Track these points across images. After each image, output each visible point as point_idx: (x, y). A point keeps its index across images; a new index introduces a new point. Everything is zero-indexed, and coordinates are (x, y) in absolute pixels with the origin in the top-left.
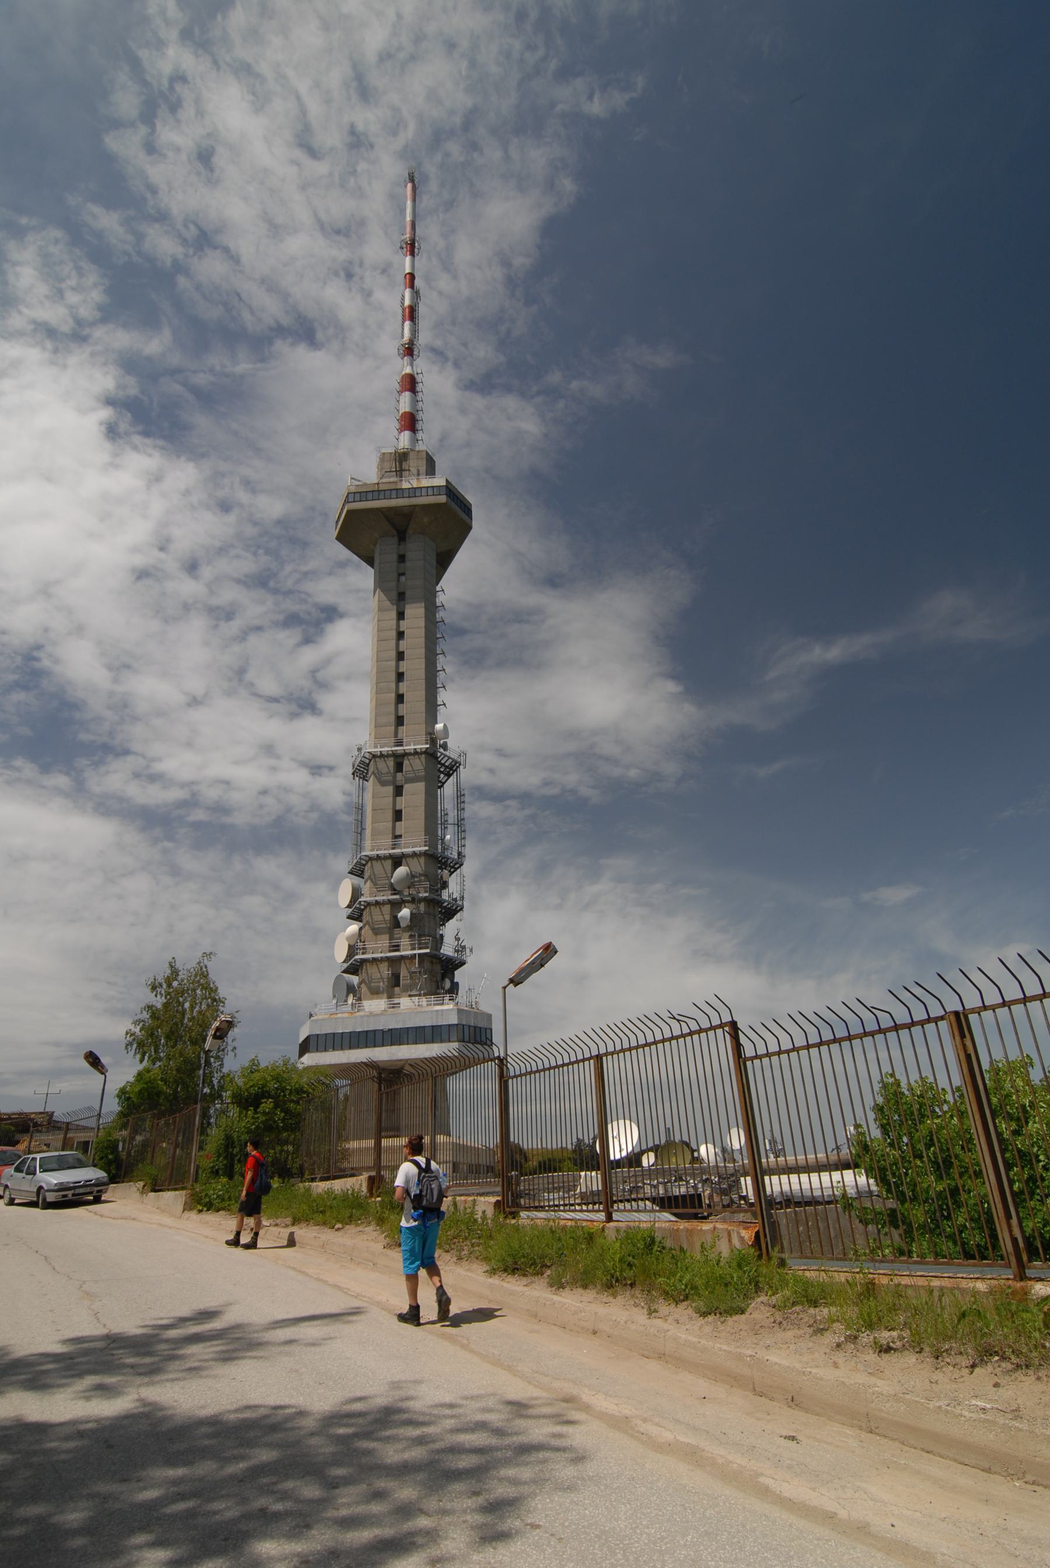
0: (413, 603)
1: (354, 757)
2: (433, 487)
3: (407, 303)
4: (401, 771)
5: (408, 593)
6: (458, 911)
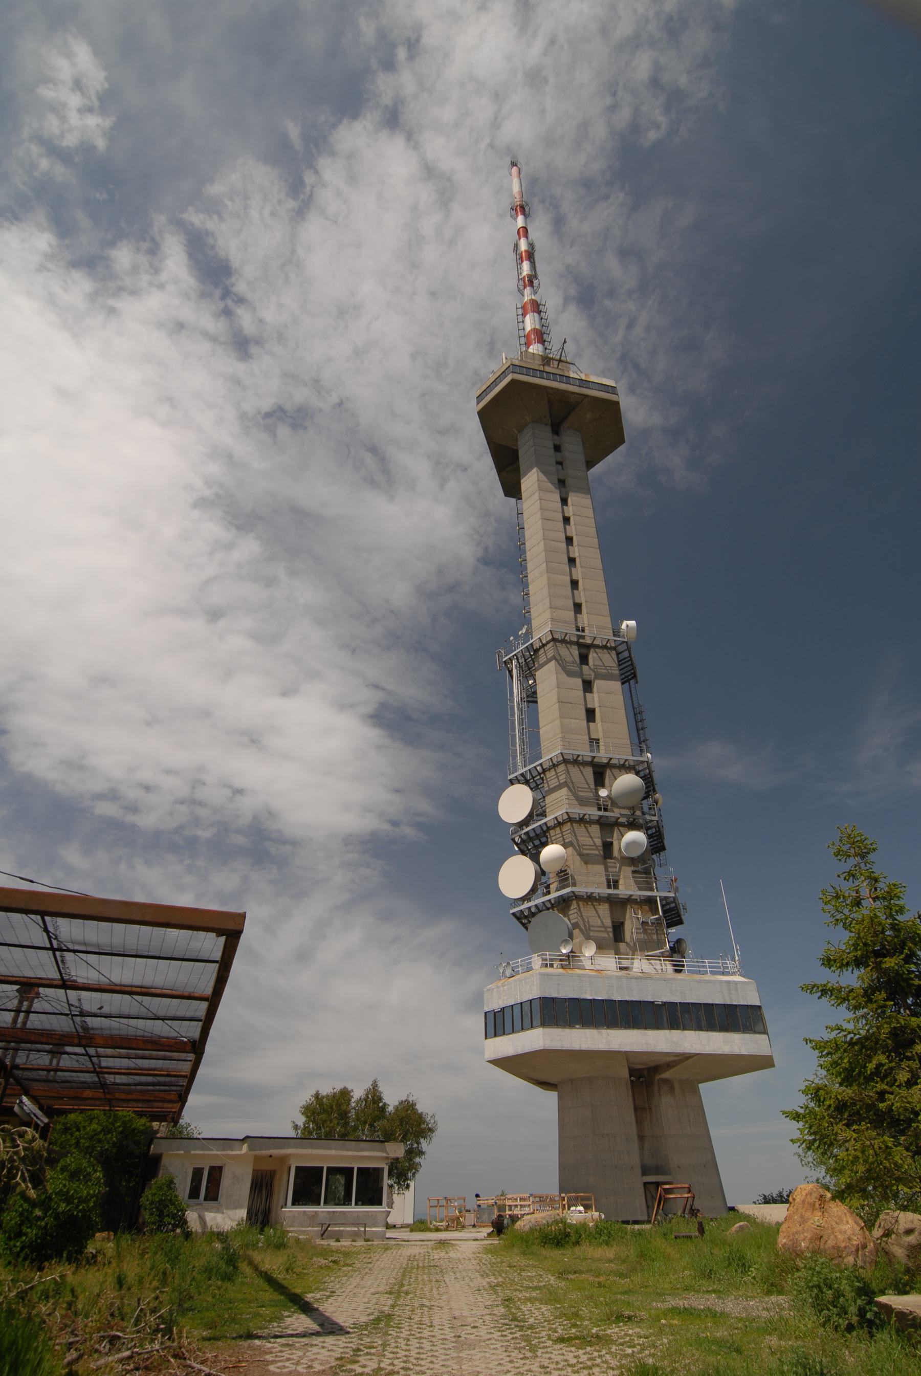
4: (587, 664)
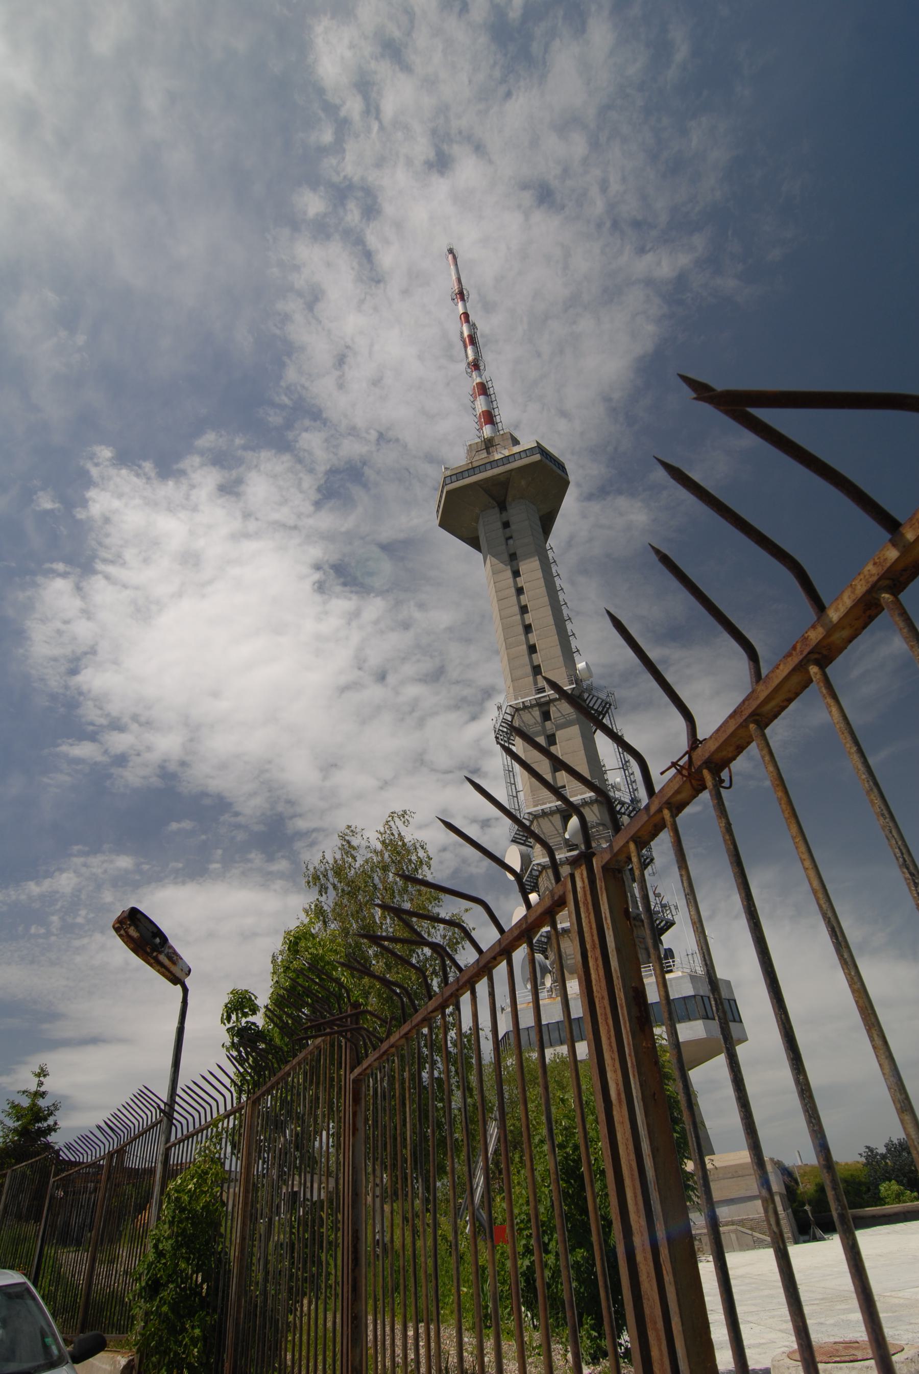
0: (525, 559)
1: (495, 720)
2: (525, 451)
3: (466, 334)
5: (519, 553)
6: (649, 864)
